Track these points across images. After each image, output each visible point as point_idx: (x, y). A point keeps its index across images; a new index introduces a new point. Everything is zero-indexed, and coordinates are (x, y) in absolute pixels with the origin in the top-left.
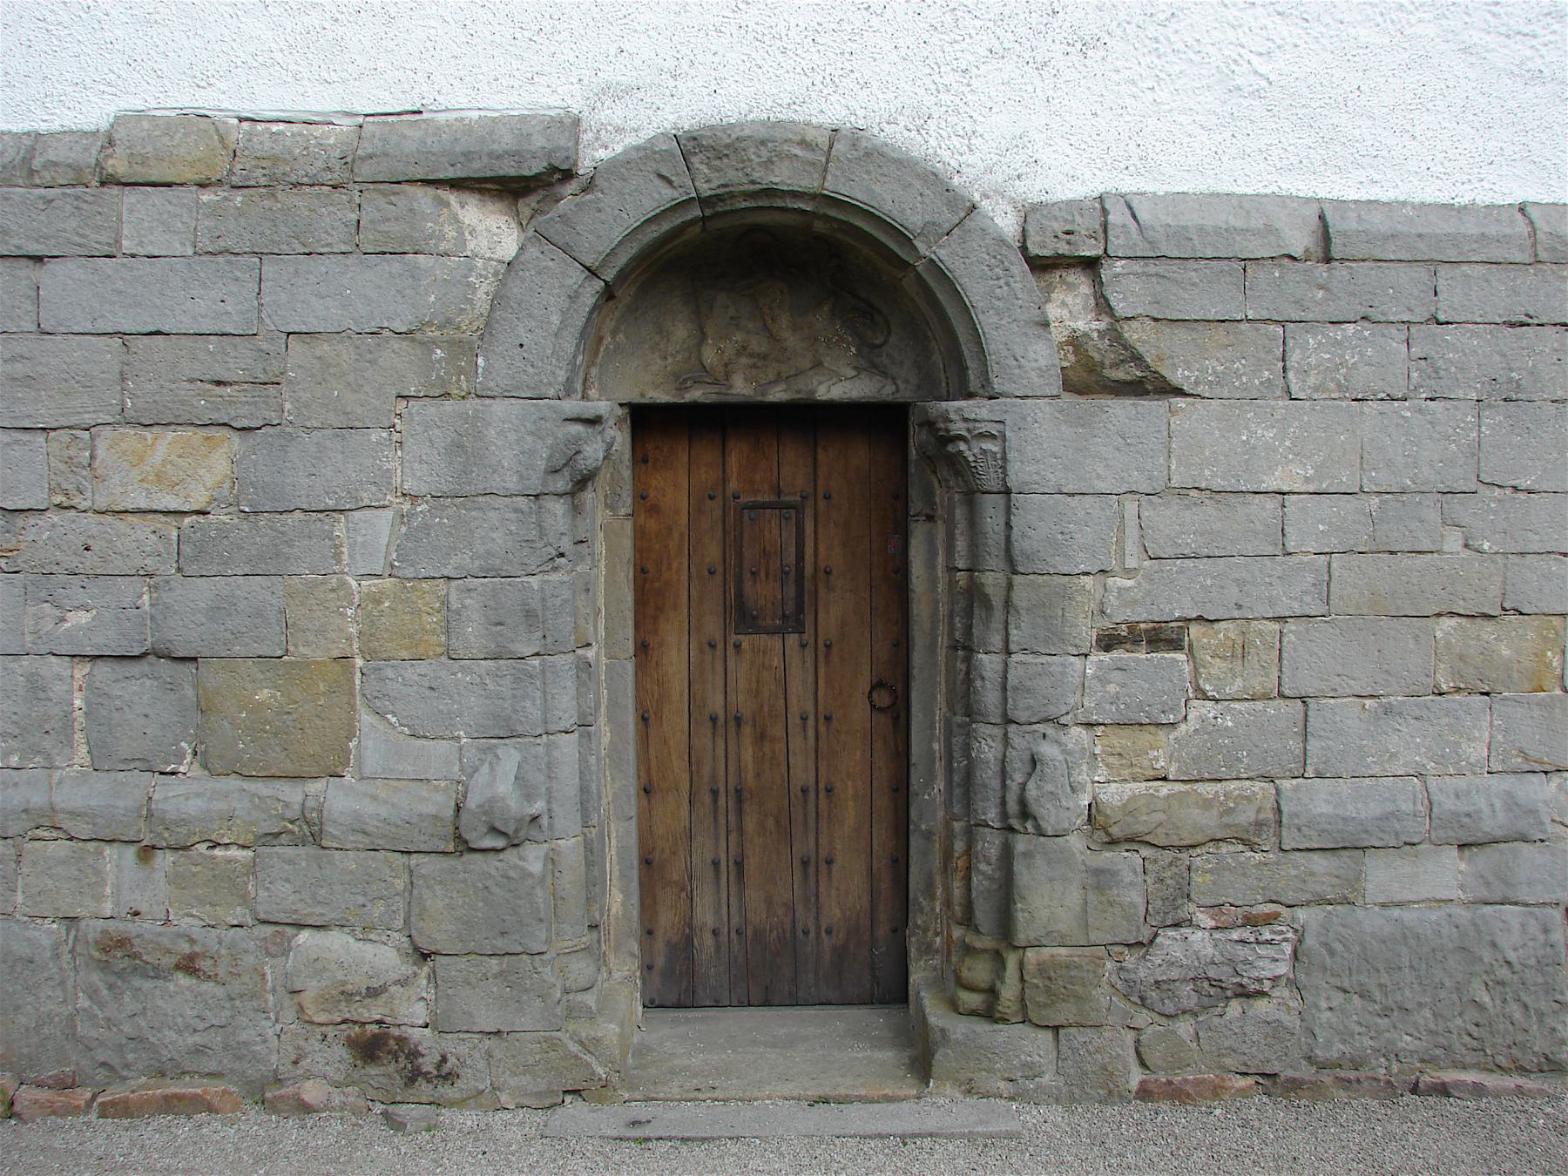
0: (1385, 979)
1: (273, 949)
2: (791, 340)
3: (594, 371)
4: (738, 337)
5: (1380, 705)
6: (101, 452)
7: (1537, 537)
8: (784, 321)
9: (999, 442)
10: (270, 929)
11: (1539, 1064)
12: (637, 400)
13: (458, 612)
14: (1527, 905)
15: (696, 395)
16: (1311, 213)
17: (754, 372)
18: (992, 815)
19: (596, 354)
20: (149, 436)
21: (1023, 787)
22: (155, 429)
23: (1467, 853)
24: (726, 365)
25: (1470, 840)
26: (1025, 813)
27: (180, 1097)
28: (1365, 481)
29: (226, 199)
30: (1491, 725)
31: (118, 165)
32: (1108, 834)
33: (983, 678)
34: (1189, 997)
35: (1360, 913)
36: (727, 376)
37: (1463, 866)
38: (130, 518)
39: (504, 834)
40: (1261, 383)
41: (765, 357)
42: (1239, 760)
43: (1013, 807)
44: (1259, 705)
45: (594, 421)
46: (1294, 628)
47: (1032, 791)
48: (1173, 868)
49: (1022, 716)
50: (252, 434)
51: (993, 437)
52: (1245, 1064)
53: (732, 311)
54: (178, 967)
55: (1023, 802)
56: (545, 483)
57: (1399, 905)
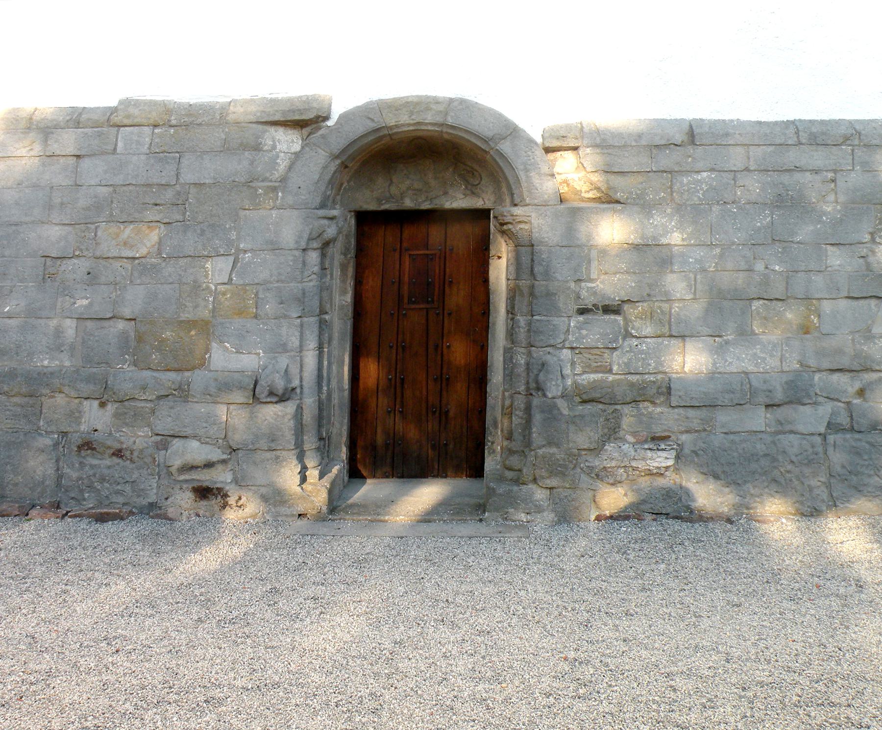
0: (727, 469)
1: (160, 447)
2: (433, 183)
3: (339, 198)
4: (408, 182)
5: (724, 340)
6: (99, 233)
7: (804, 264)
8: (430, 175)
9: (528, 225)
10: (159, 438)
11: (811, 512)
12: (358, 209)
13: (263, 299)
14: (803, 434)
15: (386, 206)
16: (686, 127)
17: (415, 197)
18: (522, 388)
19: (340, 190)
20: (122, 227)
21: (538, 375)
22: (125, 224)
23: (770, 409)
24: (402, 194)
25: (771, 403)
26: (539, 388)
27: (108, 514)
28: (713, 240)
29: (166, 131)
30: (782, 349)
31: (116, 119)
32: (581, 398)
33: (519, 327)
34: (622, 475)
35: (713, 437)
36: (402, 199)
37: (768, 415)
38: (110, 260)
39: (277, 395)
40: (660, 198)
41: (420, 190)
42: (650, 365)
43: (533, 385)
44: (660, 340)
45: (332, 219)
46: (677, 305)
47: (542, 377)
48: (614, 414)
49: (537, 344)
50: (170, 225)
51: (526, 222)
52: (652, 508)
53: (405, 172)
54: (113, 454)
55: (537, 382)
56: (308, 244)
57: (732, 433)
